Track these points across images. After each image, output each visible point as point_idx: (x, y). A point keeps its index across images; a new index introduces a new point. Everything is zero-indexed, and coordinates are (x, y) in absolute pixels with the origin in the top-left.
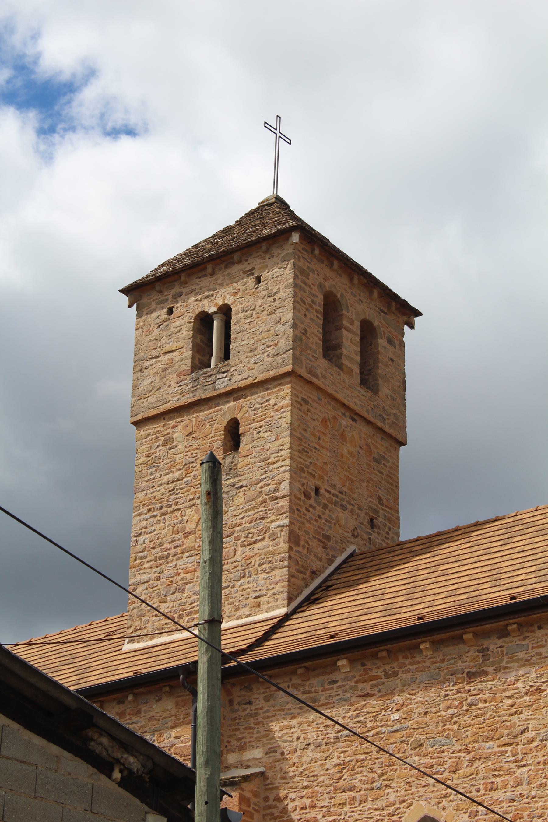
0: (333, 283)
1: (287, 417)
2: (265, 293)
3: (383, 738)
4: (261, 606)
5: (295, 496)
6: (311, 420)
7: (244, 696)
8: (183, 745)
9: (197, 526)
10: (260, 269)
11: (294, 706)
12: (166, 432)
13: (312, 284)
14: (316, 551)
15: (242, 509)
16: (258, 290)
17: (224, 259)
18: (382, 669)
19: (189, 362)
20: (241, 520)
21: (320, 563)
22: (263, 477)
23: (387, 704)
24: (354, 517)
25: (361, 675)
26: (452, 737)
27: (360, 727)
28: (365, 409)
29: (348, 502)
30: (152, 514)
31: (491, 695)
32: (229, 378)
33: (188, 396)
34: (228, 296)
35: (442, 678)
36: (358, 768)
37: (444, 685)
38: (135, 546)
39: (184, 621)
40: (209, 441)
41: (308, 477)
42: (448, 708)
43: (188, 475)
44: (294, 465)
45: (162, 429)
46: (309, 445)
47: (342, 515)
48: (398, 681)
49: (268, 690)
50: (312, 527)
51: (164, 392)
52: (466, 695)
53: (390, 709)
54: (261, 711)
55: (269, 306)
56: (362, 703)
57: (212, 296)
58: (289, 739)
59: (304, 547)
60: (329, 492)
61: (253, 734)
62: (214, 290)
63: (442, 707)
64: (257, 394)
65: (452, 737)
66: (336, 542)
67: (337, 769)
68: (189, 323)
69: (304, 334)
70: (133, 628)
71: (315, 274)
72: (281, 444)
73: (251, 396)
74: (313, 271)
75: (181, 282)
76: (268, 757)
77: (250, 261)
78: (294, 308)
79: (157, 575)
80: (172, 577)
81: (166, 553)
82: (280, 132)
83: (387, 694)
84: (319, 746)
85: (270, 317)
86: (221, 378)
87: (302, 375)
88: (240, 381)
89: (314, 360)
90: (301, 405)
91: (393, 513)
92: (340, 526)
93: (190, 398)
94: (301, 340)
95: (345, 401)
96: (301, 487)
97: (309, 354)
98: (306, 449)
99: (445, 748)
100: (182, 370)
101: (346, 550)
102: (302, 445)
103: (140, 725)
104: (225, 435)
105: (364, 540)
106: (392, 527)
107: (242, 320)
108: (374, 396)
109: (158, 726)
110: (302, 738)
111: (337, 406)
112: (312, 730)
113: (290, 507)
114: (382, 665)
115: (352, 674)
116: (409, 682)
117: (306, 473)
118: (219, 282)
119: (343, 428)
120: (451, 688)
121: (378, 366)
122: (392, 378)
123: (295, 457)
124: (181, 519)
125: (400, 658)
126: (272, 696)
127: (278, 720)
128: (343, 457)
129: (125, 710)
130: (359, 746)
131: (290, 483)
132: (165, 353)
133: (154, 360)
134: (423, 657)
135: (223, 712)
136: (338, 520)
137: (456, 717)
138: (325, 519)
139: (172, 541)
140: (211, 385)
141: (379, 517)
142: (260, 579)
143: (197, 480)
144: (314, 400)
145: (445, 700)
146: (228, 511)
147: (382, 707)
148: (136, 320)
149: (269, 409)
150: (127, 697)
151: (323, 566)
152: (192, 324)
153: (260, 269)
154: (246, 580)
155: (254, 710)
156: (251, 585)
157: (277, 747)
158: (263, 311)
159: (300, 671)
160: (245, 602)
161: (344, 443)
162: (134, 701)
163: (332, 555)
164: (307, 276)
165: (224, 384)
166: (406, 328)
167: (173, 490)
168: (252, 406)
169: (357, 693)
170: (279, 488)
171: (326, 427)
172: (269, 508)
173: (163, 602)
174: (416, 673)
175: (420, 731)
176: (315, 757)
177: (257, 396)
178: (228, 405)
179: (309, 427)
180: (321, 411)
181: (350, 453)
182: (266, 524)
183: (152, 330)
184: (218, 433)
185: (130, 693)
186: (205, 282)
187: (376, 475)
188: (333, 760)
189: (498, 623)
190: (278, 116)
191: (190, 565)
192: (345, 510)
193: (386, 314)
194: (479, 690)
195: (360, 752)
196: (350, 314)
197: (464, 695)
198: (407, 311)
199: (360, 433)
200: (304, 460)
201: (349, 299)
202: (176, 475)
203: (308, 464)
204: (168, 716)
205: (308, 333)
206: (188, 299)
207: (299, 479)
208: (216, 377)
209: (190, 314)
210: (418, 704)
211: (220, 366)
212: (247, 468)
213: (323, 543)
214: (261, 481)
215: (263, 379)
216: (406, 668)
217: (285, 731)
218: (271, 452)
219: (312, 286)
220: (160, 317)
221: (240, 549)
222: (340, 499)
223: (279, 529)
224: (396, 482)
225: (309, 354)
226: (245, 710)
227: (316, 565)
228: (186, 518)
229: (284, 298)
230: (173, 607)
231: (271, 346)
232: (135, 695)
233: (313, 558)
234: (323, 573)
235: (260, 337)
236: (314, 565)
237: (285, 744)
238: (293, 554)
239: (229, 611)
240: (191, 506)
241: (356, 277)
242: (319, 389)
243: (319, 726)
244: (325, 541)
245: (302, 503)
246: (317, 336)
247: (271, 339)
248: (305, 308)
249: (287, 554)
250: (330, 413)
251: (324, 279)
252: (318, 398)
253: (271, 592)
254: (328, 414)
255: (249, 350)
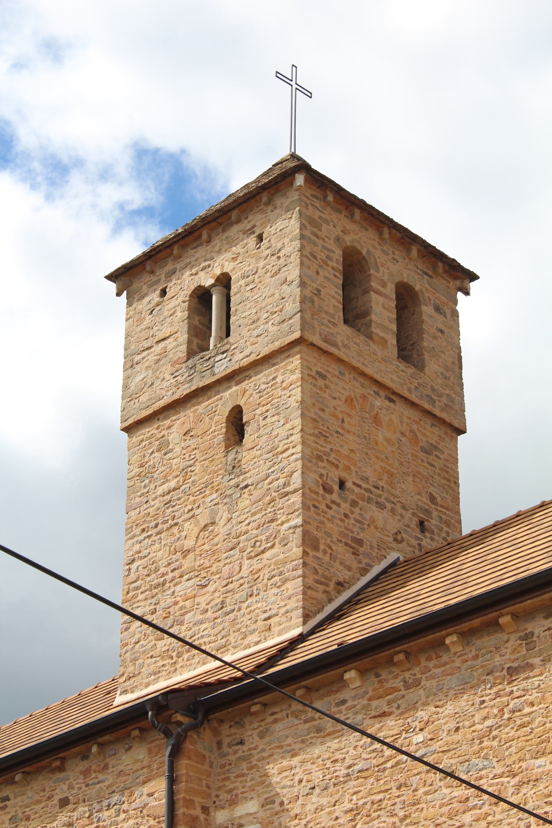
0: (355, 237)
1: (297, 394)
2: (268, 252)
3: (404, 769)
4: (272, 629)
5: (309, 489)
6: (330, 398)
7: (235, 734)
8: (157, 803)
9: (196, 542)
10: (261, 225)
11: (295, 740)
12: (161, 435)
13: (326, 237)
14: (343, 558)
15: (248, 513)
16: (260, 250)
17: (220, 220)
18: (401, 678)
19: (184, 347)
20: (246, 527)
21: (348, 573)
22: (270, 471)
23: (408, 723)
24: (397, 518)
25: (375, 690)
26: (491, 757)
27: (376, 757)
28: (405, 387)
29: (387, 500)
30: (146, 535)
31: (539, 695)
32: (229, 359)
33: (184, 387)
34: (227, 263)
35: (475, 681)
36: (374, 812)
37: (478, 689)
38: (127, 576)
39: (183, 659)
40: (209, 437)
41: (328, 466)
42: (485, 718)
43: (186, 482)
44: (308, 452)
45: (157, 431)
46: (328, 428)
47: (380, 516)
48: (421, 692)
49: (263, 723)
50: (336, 529)
51: (158, 388)
52: (507, 698)
53: (412, 730)
54: (255, 752)
55: (273, 266)
56: (377, 726)
57: (209, 266)
58: (289, 783)
59: (325, 552)
60: (359, 486)
61: (246, 782)
62: (212, 259)
63: (477, 718)
64: (262, 372)
65: (491, 757)
66: (372, 547)
67: (349, 816)
68: (184, 302)
69: (316, 294)
70: (125, 675)
71: (329, 225)
72: (290, 427)
73: (256, 376)
74: (327, 222)
75: (174, 257)
76: (265, 810)
77: (250, 218)
78: (302, 264)
79: (153, 607)
80: (169, 608)
81: (162, 579)
82: (296, 84)
83: (408, 710)
84: (326, 788)
85: (274, 279)
86: (221, 360)
87: (315, 342)
88: (241, 360)
89: (331, 326)
90: (316, 379)
91: (452, 515)
92: (376, 528)
93: (186, 389)
94: (312, 301)
95: (377, 377)
96: (318, 479)
97: (324, 318)
98: (324, 433)
99: (483, 772)
100: (177, 358)
101: (386, 557)
102: (319, 428)
103: (107, 783)
104: (227, 427)
105: (411, 546)
106: (451, 532)
107: (243, 288)
108: (418, 372)
109: (129, 782)
110: (304, 780)
111: (367, 383)
112: (317, 769)
113: (303, 503)
114: (400, 673)
115: (364, 690)
116: (435, 691)
117: (325, 461)
118: (216, 249)
119: (376, 409)
120: (488, 692)
121: (423, 337)
122: (443, 352)
123: (309, 442)
124: (179, 536)
125: (422, 660)
126: (267, 729)
127: (276, 760)
128: (377, 444)
129: (91, 766)
130: (375, 783)
131: (302, 473)
132: (158, 342)
133: (147, 352)
134: (451, 655)
135: (210, 758)
136: (373, 521)
137: (496, 729)
138: (355, 519)
139: (169, 564)
140: (210, 370)
141: (432, 519)
142: (270, 595)
143: (197, 485)
144: (335, 375)
145: (481, 709)
146: (232, 518)
147: (403, 728)
148: (126, 310)
149: (276, 389)
150: (90, 750)
151: (354, 576)
152: (187, 303)
153: (261, 225)
154: (254, 599)
155: (247, 751)
156: (259, 605)
157: (274, 795)
158: (266, 273)
159: (299, 693)
160: (253, 627)
161: (379, 428)
162: (99, 753)
163: (366, 563)
164: (319, 227)
165: (224, 367)
166: (460, 295)
167: (170, 501)
168: (257, 388)
169: (370, 714)
170: (289, 481)
171: (353, 407)
172: (279, 507)
173: (160, 640)
174: (443, 678)
175: (450, 754)
176: (321, 803)
177: (262, 375)
178: (230, 391)
179: (328, 407)
180: (344, 388)
181: (388, 440)
182: (276, 527)
183: (144, 318)
184: (219, 427)
185: (94, 744)
186: (201, 251)
187: (427, 469)
188: (342, 805)
189: (543, 597)
190: (293, 65)
191: (189, 590)
192: (383, 509)
193: (431, 277)
194: (523, 690)
195: (376, 791)
196: (381, 274)
197: (505, 699)
198: (459, 274)
199: (400, 417)
200: (322, 446)
201: (379, 258)
202: (173, 484)
203: (328, 451)
204: (139, 768)
205: (322, 293)
206: (183, 274)
207: (315, 468)
208: (214, 360)
209: (185, 292)
210: (447, 719)
211: (218, 346)
212: (252, 463)
213: (353, 548)
214: (269, 476)
215: (267, 353)
216: (430, 673)
217: (284, 774)
218: (279, 440)
219: (326, 239)
220: (152, 301)
221: (246, 562)
222: (375, 495)
223: (291, 531)
224: (454, 477)
225: (324, 318)
226: (236, 752)
227: (343, 575)
228: (183, 534)
229: (289, 254)
230: (170, 644)
231: (276, 312)
232: (101, 745)
233: (339, 566)
234: (353, 585)
235: (264, 304)
236: (340, 575)
237: (285, 791)
238: (309, 560)
239: (235, 640)
240: (190, 519)
241: (386, 231)
242: (340, 361)
243: (325, 762)
244: (356, 546)
245: (320, 498)
246: (335, 298)
247: (275, 304)
248: (317, 264)
249: (301, 561)
250: (357, 391)
251: (342, 231)
252: (340, 372)
253: (283, 610)
254: (354, 392)
255: (251, 321)
